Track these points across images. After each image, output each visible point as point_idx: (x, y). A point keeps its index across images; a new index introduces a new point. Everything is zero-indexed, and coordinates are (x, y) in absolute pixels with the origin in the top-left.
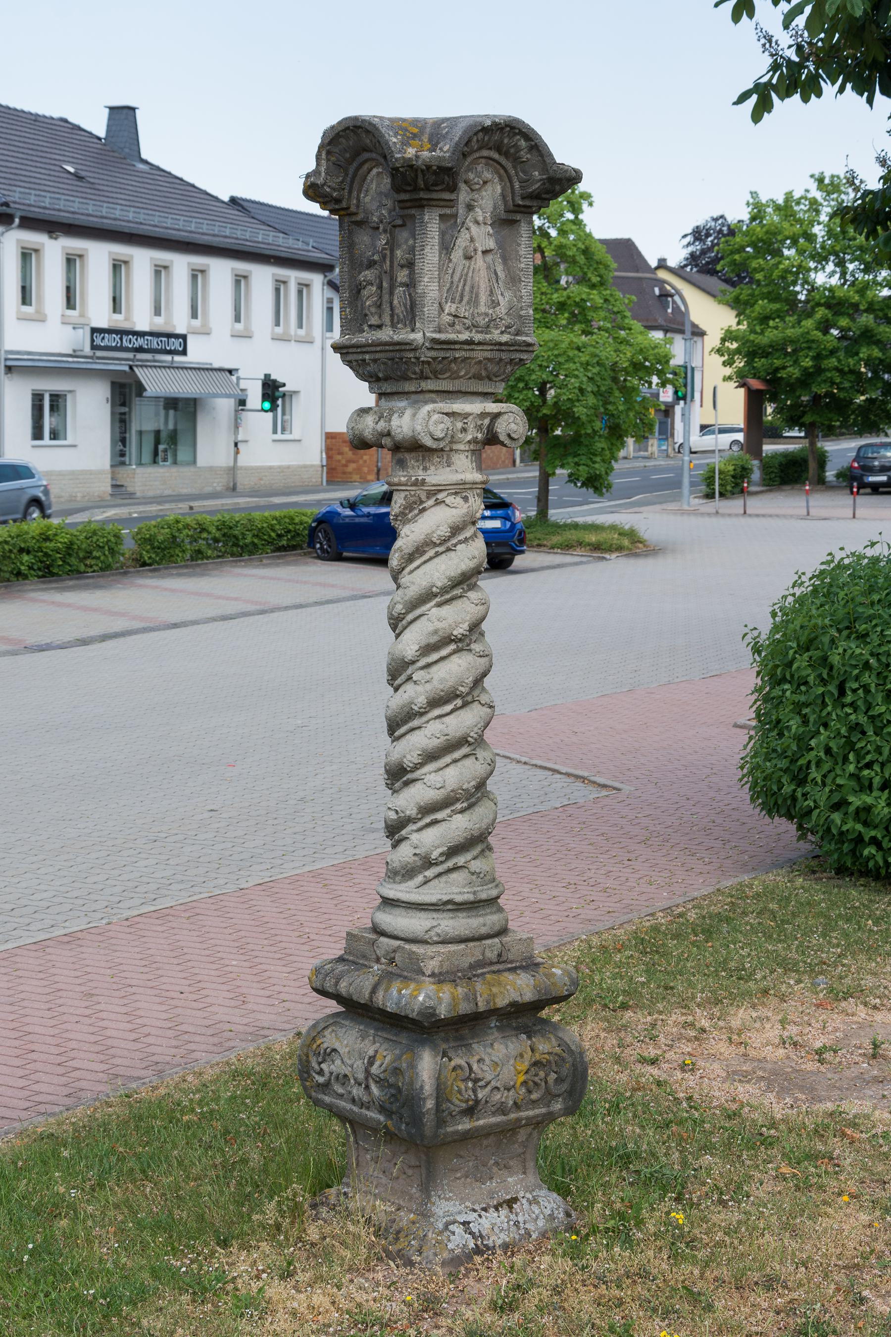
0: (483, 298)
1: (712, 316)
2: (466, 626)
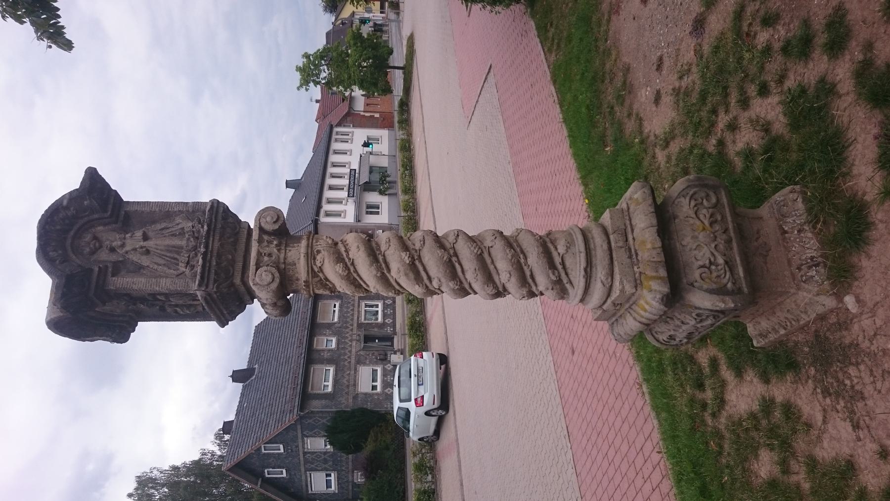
0: (177, 242)
1: (348, 10)
2: (403, 254)
